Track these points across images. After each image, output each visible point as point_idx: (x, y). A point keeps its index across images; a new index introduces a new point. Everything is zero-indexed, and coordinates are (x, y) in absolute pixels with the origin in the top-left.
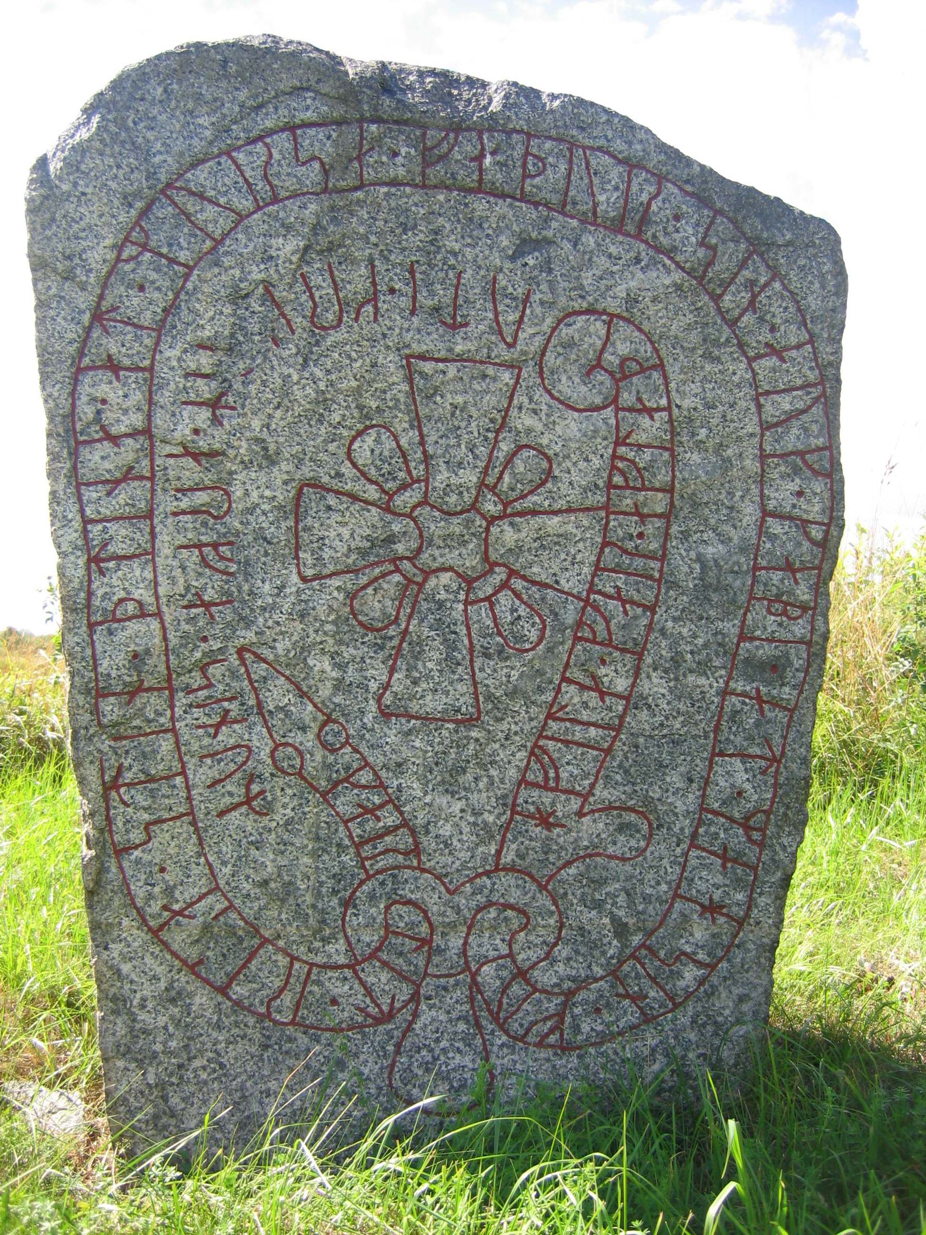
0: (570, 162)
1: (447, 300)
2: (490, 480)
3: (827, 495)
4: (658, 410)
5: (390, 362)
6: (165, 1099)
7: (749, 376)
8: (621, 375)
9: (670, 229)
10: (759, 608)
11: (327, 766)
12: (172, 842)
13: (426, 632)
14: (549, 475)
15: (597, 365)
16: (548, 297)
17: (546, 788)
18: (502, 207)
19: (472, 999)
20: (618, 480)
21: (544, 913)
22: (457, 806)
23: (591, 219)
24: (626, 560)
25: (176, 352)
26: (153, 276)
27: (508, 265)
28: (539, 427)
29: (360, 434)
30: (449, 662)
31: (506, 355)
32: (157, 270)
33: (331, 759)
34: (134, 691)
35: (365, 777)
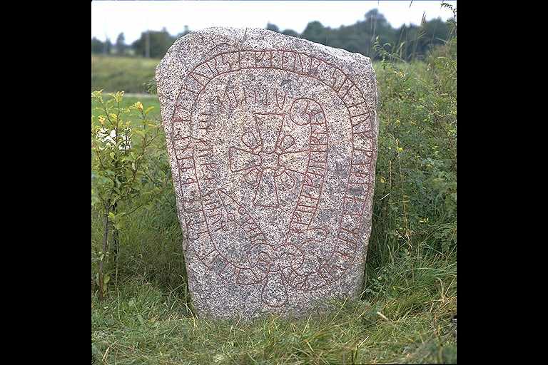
6: (206, 302)
13: (264, 184)
14: (294, 143)
18: (277, 72)
20: (312, 143)
21: (299, 255)
22: (275, 228)
23: (301, 73)
28: (290, 130)
31: (280, 112)
34: (191, 201)
35: (251, 221)
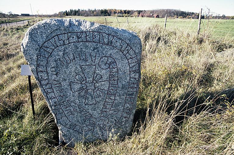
0: (100, 35)
2: (94, 79)
5: (78, 67)
7: (128, 62)
8: (110, 64)
9: (115, 44)
10: (130, 89)
15: (107, 63)
16: (99, 56)
19: (100, 128)
23: (104, 44)
24: (113, 85)
25: (49, 69)
27: (92, 52)
28: (100, 72)
30: (92, 99)
31: (94, 64)
32: (44, 58)
33: (80, 109)
35: (84, 111)
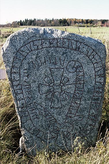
0: (69, 42)
1: (54, 61)
2: (61, 82)
3: (104, 79)
4: (82, 71)
5: (48, 69)
7: (93, 66)
8: (77, 68)
10: (95, 93)
11: (45, 114)
12: (29, 122)
14: (69, 81)
15: (74, 67)
16: (67, 60)
17: (70, 114)
19: (64, 135)
20: (77, 80)
23: (72, 49)
25: (22, 71)
26: (18, 62)
27: (62, 56)
29: (45, 78)
30: (58, 102)
31: (62, 67)
32: (19, 61)
35: (50, 115)
